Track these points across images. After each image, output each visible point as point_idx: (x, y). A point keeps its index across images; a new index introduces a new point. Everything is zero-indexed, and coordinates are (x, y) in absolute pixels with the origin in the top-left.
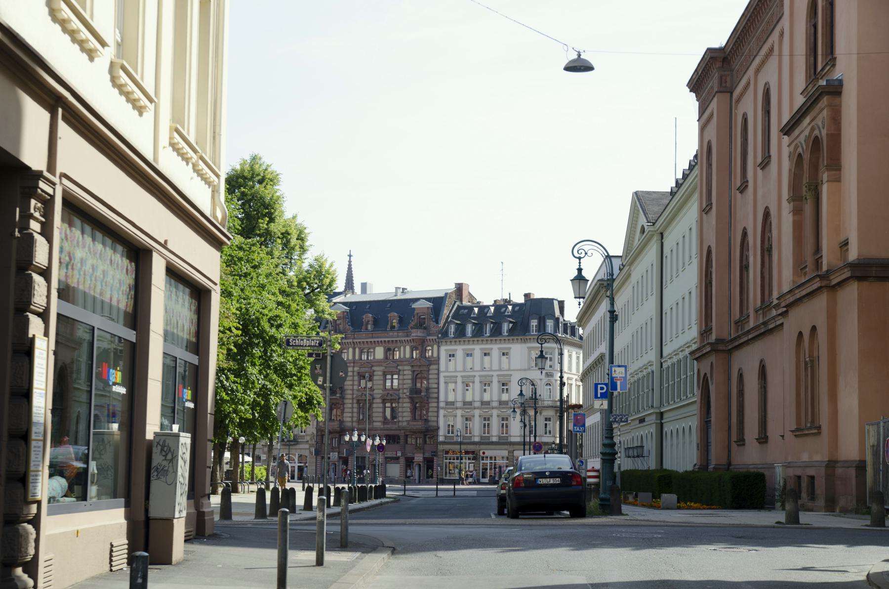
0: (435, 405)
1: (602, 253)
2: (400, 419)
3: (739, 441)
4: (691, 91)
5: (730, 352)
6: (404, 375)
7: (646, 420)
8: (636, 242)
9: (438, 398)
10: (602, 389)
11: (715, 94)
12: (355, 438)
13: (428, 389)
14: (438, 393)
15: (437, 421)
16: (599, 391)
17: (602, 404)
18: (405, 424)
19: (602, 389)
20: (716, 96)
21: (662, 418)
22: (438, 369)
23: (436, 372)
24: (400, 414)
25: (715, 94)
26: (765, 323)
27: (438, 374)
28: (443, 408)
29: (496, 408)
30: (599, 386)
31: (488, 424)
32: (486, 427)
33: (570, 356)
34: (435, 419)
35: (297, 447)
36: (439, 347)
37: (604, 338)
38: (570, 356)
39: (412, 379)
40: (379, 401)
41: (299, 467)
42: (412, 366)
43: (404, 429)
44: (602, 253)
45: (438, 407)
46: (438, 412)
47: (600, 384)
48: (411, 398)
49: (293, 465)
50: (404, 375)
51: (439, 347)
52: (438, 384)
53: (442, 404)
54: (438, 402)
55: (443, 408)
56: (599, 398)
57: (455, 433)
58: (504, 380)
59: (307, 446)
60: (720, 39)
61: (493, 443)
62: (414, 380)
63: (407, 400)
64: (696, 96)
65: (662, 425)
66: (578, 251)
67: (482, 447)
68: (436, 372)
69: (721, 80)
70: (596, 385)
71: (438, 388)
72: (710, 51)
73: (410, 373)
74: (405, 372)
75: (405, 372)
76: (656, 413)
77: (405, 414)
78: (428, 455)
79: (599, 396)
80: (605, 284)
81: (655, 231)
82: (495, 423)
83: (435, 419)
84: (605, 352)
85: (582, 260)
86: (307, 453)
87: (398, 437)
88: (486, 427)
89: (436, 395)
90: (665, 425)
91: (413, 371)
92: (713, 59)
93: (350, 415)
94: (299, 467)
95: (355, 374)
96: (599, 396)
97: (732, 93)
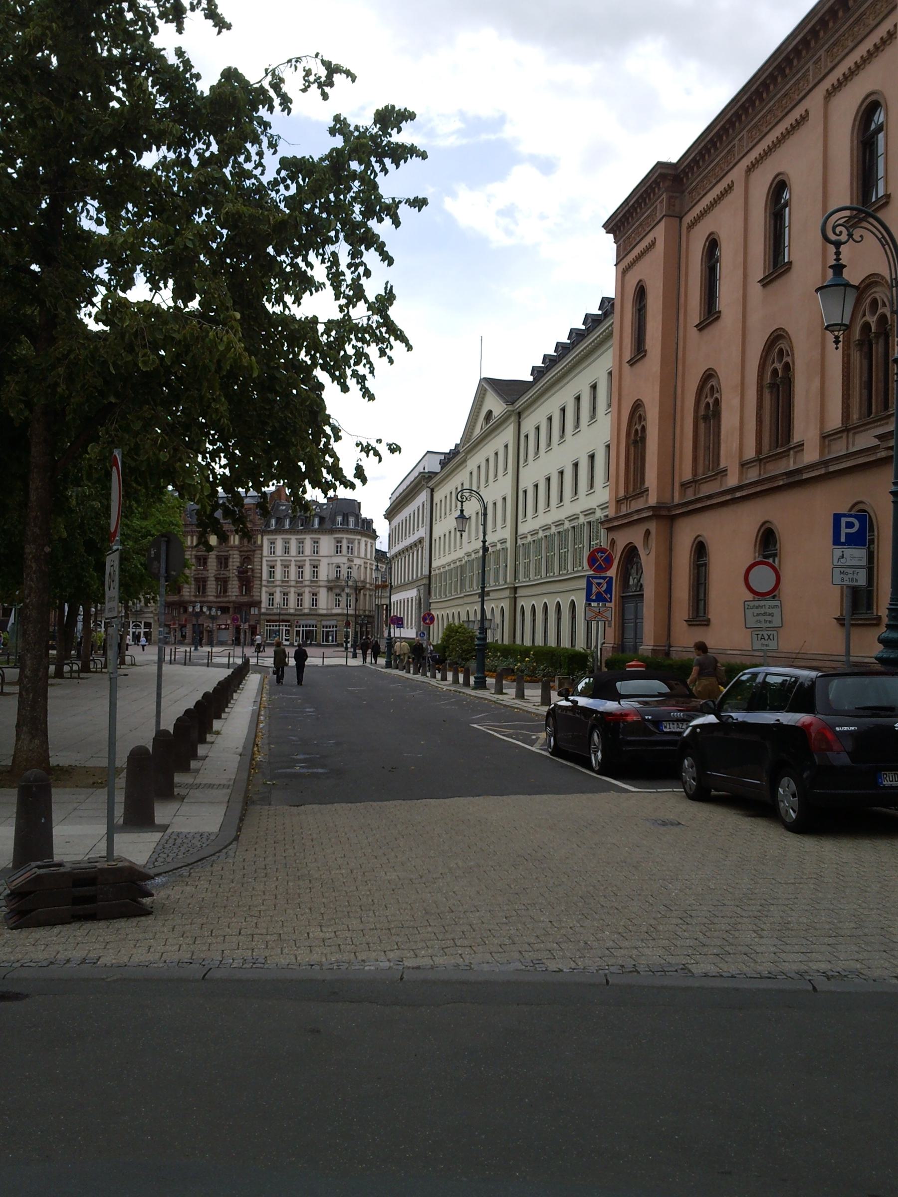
0: (259, 583)
1: (880, 236)
2: (230, 594)
3: (691, 621)
4: (607, 233)
5: (673, 518)
6: (234, 558)
7: (491, 594)
8: (477, 431)
9: (261, 577)
10: (850, 525)
11: (662, 218)
12: (198, 609)
13: (252, 570)
14: (261, 573)
15: (260, 596)
16: (844, 531)
17: (843, 557)
18: (234, 598)
19: (850, 525)
20: (664, 220)
21: (516, 593)
22: (262, 554)
23: (260, 556)
24: (230, 590)
25: (662, 218)
26: (825, 463)
27: (261, 558)
28: (265, 586)
29: (294, 587)
30: (844, 520)
31: (301, 599)
32: (300, 602)
33: (366, 545)
34: (259, 594)
35: (143, 615)
36: (262, 536)
37: (423, 523)
38: (366, 545)
39: (240, 562)
40: (213, 579)
41: (144, 632)
42: (241, 551)
43: (234, 602)
44: (880, 236)
45: (261, 585)
46: (261, 589)
47: (844, 515)
48: (238, 577)
49: (139, 630)
50: (234, 558)
51: (262, 536)
52: (261, 566)
53: (264, 583)
54: (261, 581)
55: (265, 586)
56: (843, 544)
57: (275, 606)
58: (315, 563)
59: (152, 615)
60: (673, 155)
61: (304, 615)
62: (242, 563)
63: (236, 579)
64: (615, 238)
65: (515, 598)
66: (835, 233)
67: (296, 617)
68: (260, 556)
69: (670, 205)
70: (837, 518)
71: (261, 569)
72: (659, 165)
73: (238, 556)
74: (235, 556)
75: (235, 556)
76: (510, 588)
77: (234, 590)
78: (252, 623)
79: (843, 539)
80: (427, 476)
81: (513, 411)
82: (292, 598)
83: (259, 594)
84: (424, 536)
85: (843, 248)
86: (151, 621)
87: (228, 608)
88: (300, 602)
89: (259, 575)
90: (518, 600)
91: (241, 556)
92: (663, 176)
93: (188, 590)
94: (144, 632)
95: (193, 557)
96: (843, 539)
97: (681, 219)
